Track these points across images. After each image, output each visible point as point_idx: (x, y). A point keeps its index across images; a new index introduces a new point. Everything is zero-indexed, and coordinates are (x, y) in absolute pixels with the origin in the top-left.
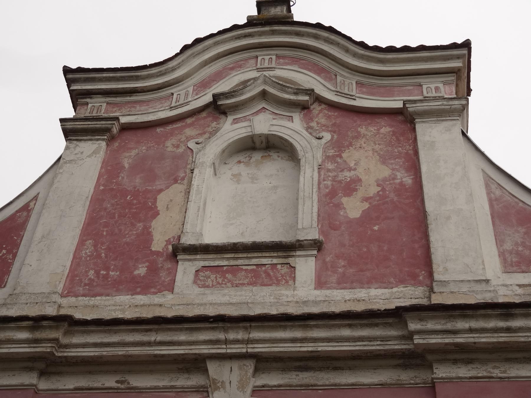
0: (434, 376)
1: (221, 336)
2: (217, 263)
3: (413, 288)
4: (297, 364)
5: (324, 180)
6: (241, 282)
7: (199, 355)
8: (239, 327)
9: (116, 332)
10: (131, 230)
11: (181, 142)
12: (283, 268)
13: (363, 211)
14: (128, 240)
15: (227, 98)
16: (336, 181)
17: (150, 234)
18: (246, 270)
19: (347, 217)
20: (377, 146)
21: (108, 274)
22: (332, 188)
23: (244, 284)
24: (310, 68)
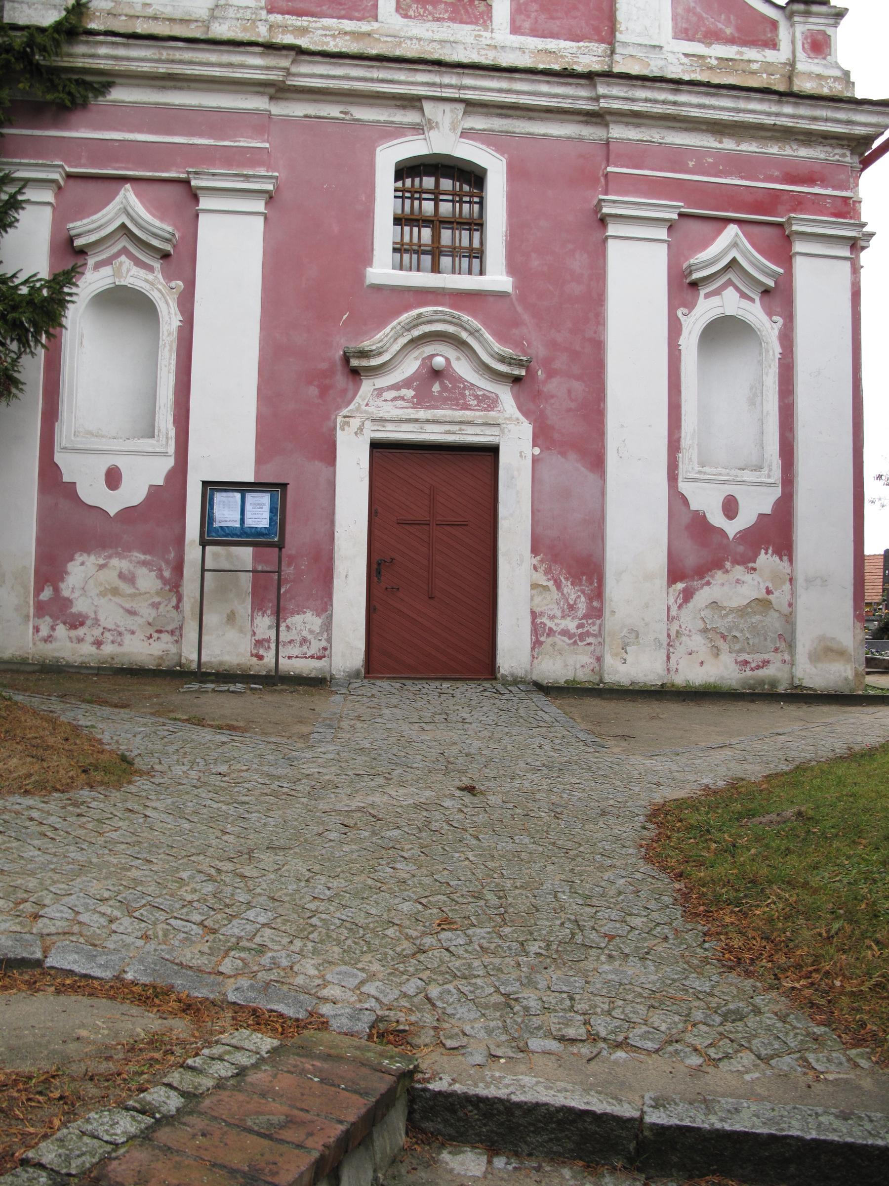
0: (610, 135)
1: (437, 79)
3: (596, 45)
4: (499, 111)
7: (417, 95)
8: (453, 73)
9: (341, 65)
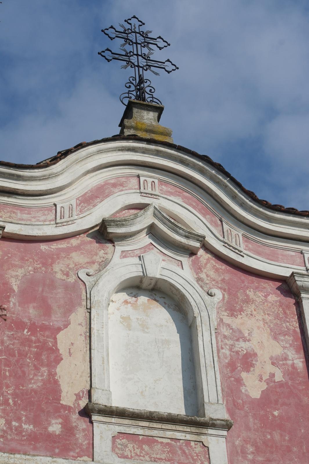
2: (132, 431)
5: (222, 348)
6: (158, 456)
10: (35, 375)
11: (70, 269)
12: (196, 446)
13: (263, 392)
14: (35, 387)
15: (117, 226)
16: (233, 352)
17: (56, 382)
18: (162, 443)
19: (248, 396)
20: (267, 316)
21: (21, 426)
22: (231, 359)
23: (162, 459)
24: (194, 204)
